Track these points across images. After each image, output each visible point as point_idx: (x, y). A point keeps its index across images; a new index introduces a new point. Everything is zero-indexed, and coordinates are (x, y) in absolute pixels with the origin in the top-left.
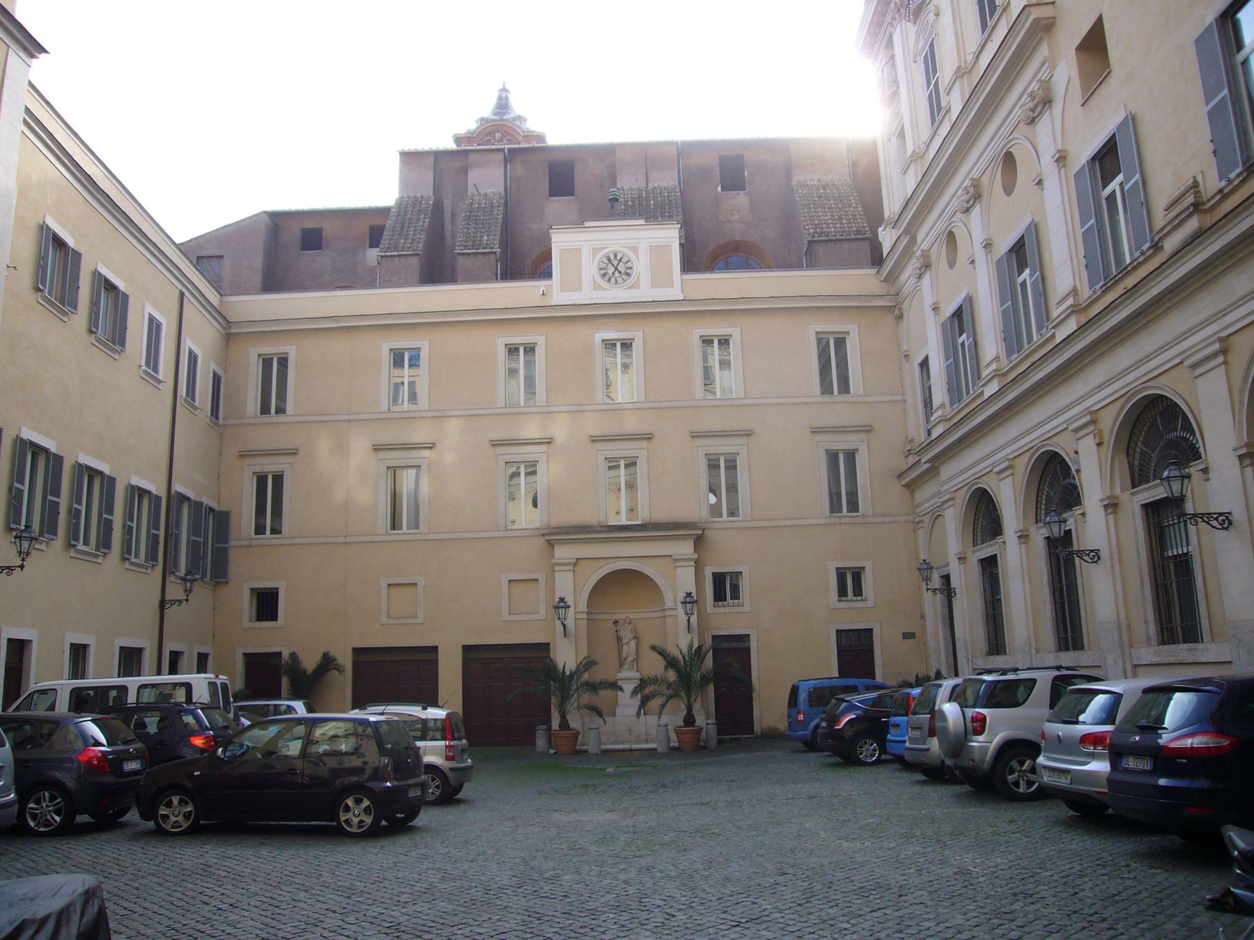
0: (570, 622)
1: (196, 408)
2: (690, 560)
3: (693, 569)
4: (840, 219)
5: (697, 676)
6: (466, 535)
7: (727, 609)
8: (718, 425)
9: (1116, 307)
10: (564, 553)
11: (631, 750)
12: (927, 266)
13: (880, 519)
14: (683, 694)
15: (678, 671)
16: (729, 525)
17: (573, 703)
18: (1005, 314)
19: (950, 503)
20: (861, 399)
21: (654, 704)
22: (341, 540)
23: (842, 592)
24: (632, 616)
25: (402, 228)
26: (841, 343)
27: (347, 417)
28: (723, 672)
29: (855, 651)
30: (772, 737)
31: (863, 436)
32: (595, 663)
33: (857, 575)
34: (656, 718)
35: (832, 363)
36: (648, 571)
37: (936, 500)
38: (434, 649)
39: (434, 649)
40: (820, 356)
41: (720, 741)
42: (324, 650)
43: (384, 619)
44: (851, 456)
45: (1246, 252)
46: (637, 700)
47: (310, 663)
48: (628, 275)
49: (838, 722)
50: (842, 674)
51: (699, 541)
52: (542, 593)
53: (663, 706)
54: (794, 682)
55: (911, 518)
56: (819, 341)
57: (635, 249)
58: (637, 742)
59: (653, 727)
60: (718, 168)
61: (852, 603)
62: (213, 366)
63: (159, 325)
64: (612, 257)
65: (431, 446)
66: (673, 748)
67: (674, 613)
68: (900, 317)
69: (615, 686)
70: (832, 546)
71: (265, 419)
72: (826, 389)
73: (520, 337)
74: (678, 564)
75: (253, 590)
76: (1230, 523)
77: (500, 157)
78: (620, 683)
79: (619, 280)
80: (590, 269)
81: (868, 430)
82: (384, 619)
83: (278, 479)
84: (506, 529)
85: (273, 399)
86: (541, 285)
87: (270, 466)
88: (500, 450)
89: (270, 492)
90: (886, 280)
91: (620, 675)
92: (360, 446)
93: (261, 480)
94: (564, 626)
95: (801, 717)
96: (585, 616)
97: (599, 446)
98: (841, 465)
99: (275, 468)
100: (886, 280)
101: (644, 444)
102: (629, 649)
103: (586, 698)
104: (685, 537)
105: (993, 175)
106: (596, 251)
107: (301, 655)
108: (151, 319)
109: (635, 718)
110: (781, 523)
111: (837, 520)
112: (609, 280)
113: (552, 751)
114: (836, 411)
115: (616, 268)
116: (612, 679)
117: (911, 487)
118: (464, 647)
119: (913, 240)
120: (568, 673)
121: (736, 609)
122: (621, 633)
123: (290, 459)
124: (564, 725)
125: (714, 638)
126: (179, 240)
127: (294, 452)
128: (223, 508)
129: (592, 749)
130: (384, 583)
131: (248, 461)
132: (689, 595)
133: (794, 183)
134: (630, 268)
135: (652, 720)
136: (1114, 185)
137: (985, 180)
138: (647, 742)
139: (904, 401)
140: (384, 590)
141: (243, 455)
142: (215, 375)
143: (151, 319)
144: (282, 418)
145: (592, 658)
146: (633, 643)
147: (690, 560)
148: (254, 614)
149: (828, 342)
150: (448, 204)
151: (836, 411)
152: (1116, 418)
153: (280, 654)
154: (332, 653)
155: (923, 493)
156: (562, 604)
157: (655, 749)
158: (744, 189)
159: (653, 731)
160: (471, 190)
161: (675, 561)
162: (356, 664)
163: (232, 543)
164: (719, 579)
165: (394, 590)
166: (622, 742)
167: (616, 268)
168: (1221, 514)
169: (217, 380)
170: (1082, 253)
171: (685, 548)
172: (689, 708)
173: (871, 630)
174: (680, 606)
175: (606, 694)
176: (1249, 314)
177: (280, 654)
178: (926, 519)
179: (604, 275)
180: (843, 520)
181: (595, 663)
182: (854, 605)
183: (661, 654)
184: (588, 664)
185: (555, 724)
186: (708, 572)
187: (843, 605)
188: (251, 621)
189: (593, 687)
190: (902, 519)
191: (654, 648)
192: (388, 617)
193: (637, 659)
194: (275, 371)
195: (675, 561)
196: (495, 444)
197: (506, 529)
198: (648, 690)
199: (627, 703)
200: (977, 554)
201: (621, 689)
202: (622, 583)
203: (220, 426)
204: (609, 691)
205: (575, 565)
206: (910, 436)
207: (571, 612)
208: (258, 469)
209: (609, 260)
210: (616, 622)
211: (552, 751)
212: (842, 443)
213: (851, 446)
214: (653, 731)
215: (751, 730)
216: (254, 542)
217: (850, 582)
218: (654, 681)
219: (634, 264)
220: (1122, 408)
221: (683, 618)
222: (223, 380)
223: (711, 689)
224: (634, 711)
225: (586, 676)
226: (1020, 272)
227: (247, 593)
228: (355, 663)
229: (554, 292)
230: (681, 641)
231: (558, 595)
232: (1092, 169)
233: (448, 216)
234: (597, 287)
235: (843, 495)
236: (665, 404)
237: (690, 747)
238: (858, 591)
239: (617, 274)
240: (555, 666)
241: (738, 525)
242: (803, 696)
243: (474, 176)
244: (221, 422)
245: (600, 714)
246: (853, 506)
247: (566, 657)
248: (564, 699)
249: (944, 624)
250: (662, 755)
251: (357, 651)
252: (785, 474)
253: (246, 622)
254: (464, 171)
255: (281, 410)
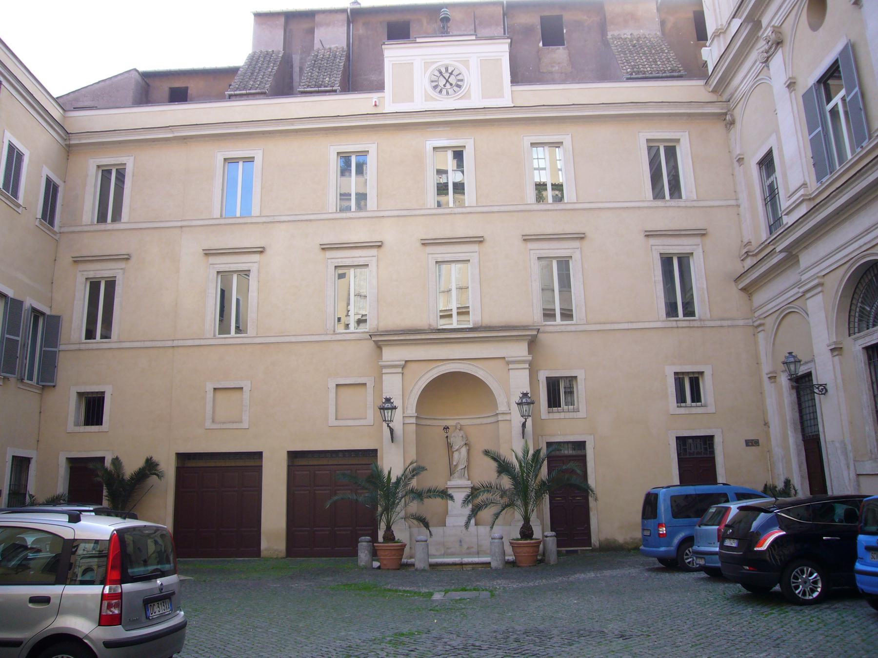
0: (397, 425)
1: (19, 206)
2: (524, 362)
3: (527, 372)
4: (655, 62)
5: (533, 484)
6: (293, 339)
7: (562, 415)
8: (550, 229)
9: (817, 210)
10: (392, 355)
11: (462, 564)
12: (779, 43)
13: (718, 323)
14: (519, 502)
15: (514, 477)
16: (563, 328)
17: (400, 511)
18: (814, 143)
19: (819, 289)
20: (695, 204)
21: (486, 514)
22: (170, 343)
23: (681, 399)
24: (463, 422)
25: (252, 74)
26: (671, 152)
27: (179, 224)
28: (559, 482)
29: (696, 456)
30: (613, 551)
31: (697, 240)
32: (423, 469)
33: (695, 380)
34: (488, 528)
35: (664, 174)
36: (480, 374)
37: (795, 290)
38: (259, 455)
39: (259, 455)
40: (651, 163)
41: (559, 553)
42: (148, 455)
43: (208, 424)
44: (684, 260)
45: (873, 196)
46: (467, 510)
47: (131, 466)
48: (459, 86)
49: (757, 543)
50: (683, 481)
51: (533, 343)
52: (370, 398)
53: (497, 515)
54: (648, 489)
55: (750, 322)
56: (650, 148)
57: (466, 63)
58: (469, 554)
59: (489, 538)
60: (539, 27)
61: (691, 409)
62: (46, 171)
63: (20, 156)
64: (443, 70)
65: (261, 251)
66: (508, 563)
67: (507, 417)
68: (732, 123)
69: (445, 494)
70: (671, 350)
71: (102, 226)
72: (658, 194)
73: (350, 145)
74: (511, 366)
75: (80, 394)
76: (826, 391)
77: (343, 17)
78: (450, 492)
79: (450, 91)
80: (421, 82)
81: (702, 234)
82: (208, 424)
83: (111, 285)
84: (334, 333)
85: (109, 207)
86: (375, 96)
87: (103, 271)
88: (330, 254)
89: (102, 297)
90: (714, 91)
91: (450, 484)
92: (190, 248)
93: (94, 286)
94: (392, 431)
95: (663, 530)
96: (413, 420)
97: (430, 249)
98: (675, 270)
99: (107, 274)
100: (714, 91)
101: (475, 247)
102: (460, 456)
103: (414, 507)
104: (518, 338)
105: (798, 17)
106: (427, 64)
107: (123, 459)
108: (11, 148)
109: (464, 528)
110: (616, 326)
111: (674, 324)
112: (441, 92)
113: (376, 564)
114: (668, 215)
115: (447, 80)
116: (441, 487)
117: (748, 291)
118: (289, 453)
119: (758, 25)
120: (394, 480)
121: (571, 415)
122: (451, 440)
123: (122, 265)
124: (389, 536)
125: (549, 444)
126: (57, 92)
127: (127, 258)
128: (54, 313)
129: (419, 565)
130: (210, 387)
131: (82, 267)
132: (525, 395)
133: (609, 37)
134: (462, 80)
135: (483, 530)
136: (837, 100)
137: (787, 28)
138: (478, 554)
139: (738, 206)
140: (210, 394)
141: (77, 261)
142: (49, 181)
143: (11, 148)
144: (117, 226)
145: (422, 464)
146: (464, 450)
147: (524, 362)
148: (83, 419)
149: (658, 149)
150: (296, 59)
151: (668, 215)
152: (842, 280)
153: (102, 459)
154: (156, 458)
155: (760, 297)
156: (387, 406)
157: (490, 563)
158: (563, 45)
159: (486, 543)
160: (317, 45)
161: (508, 363)
162: (179, 470)
163: (62, 347)
164: (553, 385)
165: (220, 395)
166: (453, 555)
167: (447, 80)
168: (821, 385)
169: (51, 190)
170: (810, 154)
171: (520, 350)
172: (527, 520)
173: (711, 438)
174: (515, 409)
175: (433, 505)
176: (875, 238)
177: (102, 459)
178: (770, 322)
179: (435, 87)
180: (681, 324)
181: (423, 469)
182: (694, 410)
183: (494, 459)
184: (417, 471)
185: (381, 534)
186: (542, 376)
187: (682, 411)
188: (77, 424)
189: (419, 495)
190: (741, 322)
191: (487, 453)
192: (213, 422)
193: (468, 467)
194: (112, 181)
195: (508, 363)
196: (325, 248)
197: (334, 333)
198: (478, 500)
199: (457, 510)
200: (861, 341)
201: (451, 497)
202: (451, 387)
203: (55, 233)
204: (439, 500)
205: (403, 367)
206: (746, 241)
207: (398, 415)
208: (91, 275)
209: (441, 73)
210: (446, 428)
211: (376, 564)
212: (675, 247)
213: (687, 250)
214: (486, 543)
215: (587, 541)
216: (83, 347)
217: (689, 387)
218: (488, 488)
219: (465, 75)
220: (846, 272)
221: (517, 419)
222: (60, 189)
223: (547, 498)
224: (463, 521)
225: (414, 483)
226: (829, 100)
227: (73, 398)
228: (178, 470)
229: (388, 102)
230: (514, 448)
231: (386, 395)
232: (818, 90)
233: (296, 69)
234: (428, 98)
235: (679, 303)
236: (496, 209)
237: (527, 561)
238: (696, 397)
239: (448, 86)
240: (381, 471)
241: (573, 328)
242: (663, 507)
243: (320, 34)
244: (56, 229)
245: (427, 525)
246: (689, 311)
247: (393, 463)
248: (388, 509)
249: (795, 429)
250: (498, 573)
251: (182, 457)
252: (618, 281)
253: (71, 427)
254: (311, 31)
255: (117, 217)
